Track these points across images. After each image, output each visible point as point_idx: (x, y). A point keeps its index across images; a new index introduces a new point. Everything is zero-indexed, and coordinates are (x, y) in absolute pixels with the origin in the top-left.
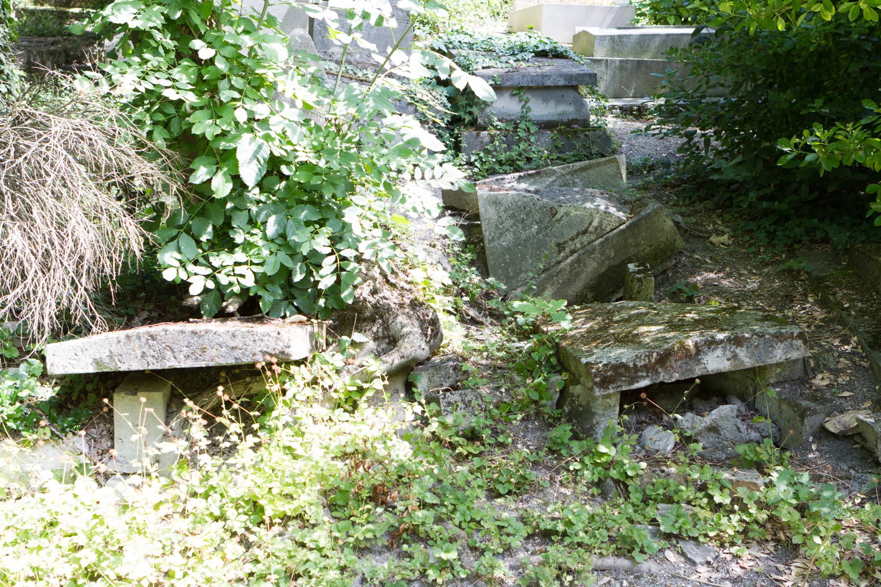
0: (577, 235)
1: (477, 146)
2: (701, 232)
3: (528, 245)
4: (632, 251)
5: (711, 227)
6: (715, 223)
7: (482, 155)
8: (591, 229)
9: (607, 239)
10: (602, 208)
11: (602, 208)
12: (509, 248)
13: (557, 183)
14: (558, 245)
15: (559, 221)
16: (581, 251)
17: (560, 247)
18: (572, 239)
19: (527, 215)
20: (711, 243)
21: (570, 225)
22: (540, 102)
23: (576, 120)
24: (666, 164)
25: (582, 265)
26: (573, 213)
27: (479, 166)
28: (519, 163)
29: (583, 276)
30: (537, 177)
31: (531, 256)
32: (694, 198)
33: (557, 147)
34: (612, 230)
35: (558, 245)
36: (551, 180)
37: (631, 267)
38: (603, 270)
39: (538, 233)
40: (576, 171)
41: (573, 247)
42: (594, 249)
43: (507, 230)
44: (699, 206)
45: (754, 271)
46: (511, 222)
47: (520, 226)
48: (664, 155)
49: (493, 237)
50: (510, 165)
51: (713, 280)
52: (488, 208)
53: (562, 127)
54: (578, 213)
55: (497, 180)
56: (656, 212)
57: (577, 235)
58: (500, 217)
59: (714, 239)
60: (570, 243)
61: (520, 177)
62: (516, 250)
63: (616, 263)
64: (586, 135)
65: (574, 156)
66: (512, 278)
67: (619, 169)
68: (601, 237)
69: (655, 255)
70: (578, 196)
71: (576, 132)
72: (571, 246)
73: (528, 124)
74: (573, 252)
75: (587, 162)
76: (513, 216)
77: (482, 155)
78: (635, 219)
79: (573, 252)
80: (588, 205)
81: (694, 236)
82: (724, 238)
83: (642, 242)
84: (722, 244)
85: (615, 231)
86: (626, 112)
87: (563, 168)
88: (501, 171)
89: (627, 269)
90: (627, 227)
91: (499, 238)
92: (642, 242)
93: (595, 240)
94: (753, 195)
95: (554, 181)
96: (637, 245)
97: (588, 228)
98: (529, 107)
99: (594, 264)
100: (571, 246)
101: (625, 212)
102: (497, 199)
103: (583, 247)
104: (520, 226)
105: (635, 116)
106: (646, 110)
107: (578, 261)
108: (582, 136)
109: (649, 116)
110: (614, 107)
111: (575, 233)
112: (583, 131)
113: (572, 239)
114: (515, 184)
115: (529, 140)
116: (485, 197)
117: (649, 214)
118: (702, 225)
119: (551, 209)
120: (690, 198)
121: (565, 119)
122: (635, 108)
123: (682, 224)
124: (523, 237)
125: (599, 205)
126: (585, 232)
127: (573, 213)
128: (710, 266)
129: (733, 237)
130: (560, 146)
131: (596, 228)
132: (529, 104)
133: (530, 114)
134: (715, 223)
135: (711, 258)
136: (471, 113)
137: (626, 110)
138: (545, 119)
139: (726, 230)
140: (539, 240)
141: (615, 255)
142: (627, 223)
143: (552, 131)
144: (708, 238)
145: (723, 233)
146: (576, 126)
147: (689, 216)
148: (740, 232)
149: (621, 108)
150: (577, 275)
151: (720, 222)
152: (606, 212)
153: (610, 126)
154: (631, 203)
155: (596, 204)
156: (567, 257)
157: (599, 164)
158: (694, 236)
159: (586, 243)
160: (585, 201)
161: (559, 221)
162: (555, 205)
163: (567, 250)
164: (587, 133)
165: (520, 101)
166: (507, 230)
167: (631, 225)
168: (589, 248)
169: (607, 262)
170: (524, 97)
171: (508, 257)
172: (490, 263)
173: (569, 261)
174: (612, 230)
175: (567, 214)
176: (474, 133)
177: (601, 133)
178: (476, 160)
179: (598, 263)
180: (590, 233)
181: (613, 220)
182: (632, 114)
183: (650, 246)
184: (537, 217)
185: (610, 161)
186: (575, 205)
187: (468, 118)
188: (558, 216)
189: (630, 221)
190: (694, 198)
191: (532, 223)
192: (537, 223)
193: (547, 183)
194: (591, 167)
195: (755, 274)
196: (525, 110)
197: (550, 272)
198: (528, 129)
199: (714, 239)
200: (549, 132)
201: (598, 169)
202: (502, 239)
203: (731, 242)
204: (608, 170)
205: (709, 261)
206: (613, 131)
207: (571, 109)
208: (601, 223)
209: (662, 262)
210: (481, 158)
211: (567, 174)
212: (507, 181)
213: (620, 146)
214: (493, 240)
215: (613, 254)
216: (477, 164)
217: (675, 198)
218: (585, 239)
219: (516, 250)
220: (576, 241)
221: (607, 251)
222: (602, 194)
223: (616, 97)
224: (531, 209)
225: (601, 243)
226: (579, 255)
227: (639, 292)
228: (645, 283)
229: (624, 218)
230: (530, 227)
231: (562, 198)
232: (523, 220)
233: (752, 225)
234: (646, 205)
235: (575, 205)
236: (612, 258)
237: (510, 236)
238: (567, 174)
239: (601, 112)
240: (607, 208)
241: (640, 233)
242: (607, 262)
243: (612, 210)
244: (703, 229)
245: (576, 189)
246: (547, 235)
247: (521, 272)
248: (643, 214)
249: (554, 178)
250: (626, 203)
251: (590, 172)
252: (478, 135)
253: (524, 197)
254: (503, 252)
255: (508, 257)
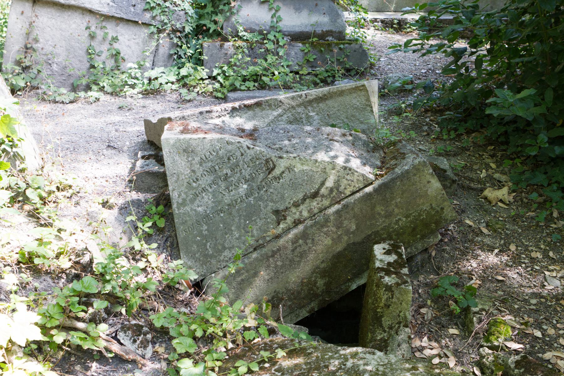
0: (304, 200)
1: (220, 58)
2: (471, 180)
3: (234, 212)
4: (381, 223)
5: (483, 174)
6: (488, 167)
7: (225, 68)
8: (323, 191)
9: (346, 206)
10: (340, 161)
11: (340, 161)
12: (207, 216)
13: (285, 118)
14: (277, 212)
15: (277, 178)
16: (309, 223)
17: (280, 215)
18: (296, 205)
19: (232, 170)
20: (486, 198)
21: (294, 186)
22: (292, 11)
23: (331, 31)
24: (428, 88)
25: (309, 241)
26: (299, 167)
27: (221, 80)
28: (264, 78)
29: (311, 256)
30: (257, 110)
31: (238, 228)
32: (461, 130)
33: (308, 61)
34: (353, 193)
35: (277, 212)
36: (275, 113)
37: (378, 250)
38: (339, 248)
39: (247, 196)
40: (310, 102)
41: (297, 216)
42: (327, 220)
43: (204, 190)
44: (467, 141)
45: (551, 254)
46: (209, 179)
47: (223, 185)
48: (423, 71)
49: (184, 200)
50: (255, 81)
51: (494, 267)
52: (177, 158)
53: (315, 39)
54: (305, 168)
55: (201, 113)
56: (416, 169)
57: (304, 200)
58: (194, 171)
59: (489, 193)
60: (294, 210)
61: (234, 109)
62: (218, 218)
63: (358, 239)
64: (340, 49)
65: (327, 71)
66: (212, 256)
67: (368, 100)
68: (338, 202)
69: (414, 229)
70: (309, 140)
71: (329, 45)
72: (294, 214)
73: (277, 35)
74: (297, 223)
75: (326, 89)
76: (213, 171)
77: (225, 68)
78: (386, 179)
79: (297, 223)
80: (322, 156)
81: (463, 187)
82: (503, 193)
83: (396, 210)
84: (501, 201)
85: (358, 195)
86: (387, 25)
87: (293, 98)
88: (243, 88)
89: (370, 257)
90: (376, 190)
91: (192, 201)
92: (396, 210)
93: (329, 207)
94: (543, 137)
95: (280, 116)
96: (389, 215)
97: (319, 189)
98: (279, 17)
99: (328, 241)
100: (294, 214)
101: (373, 166)
102: (189, 145)
103: (312, 216)
104: (223, 185)
105: (395, 29)
106: (406, 23)
107: (304, 235)
108: (336, 50)
109: (409, 30)
110: (375, 20)
111: (301, 196)
112: (337, 44)
113: (296, 205)
114: (227, 119)
115: (278, 54)
116: (172, 142)
117: (407, 172)
118: (472, 170)
119: (267, 161)
120: (456, 130)
121: (319, 30)
122: (396, 21)
123: (449, 173)
124: (227, 199)
125: (336, 157)
126: (315, 195)
127: (299, 167)
128: (487, 241)
129: (514, 191)
130: (311, 60)
131: (331, 190)
132: (279, 13)
133: (280, 24)
134: (488, 167)
135: (487, 226)
136: (216, 22)
137: (386, 23)
138: (298, 29)
139: (503, 178)
140: (249, 205)
141: (357, 229)
142: (376, 184)
143: (304, 44)
144: (482, 190)
145: (499, 185)
146: (330, 38)
147: (455, 155)
148: (523, 185)
149: (382, 21)
150: (302, 255)
151: (493, 166)
152: (345, 168)
153: (369, 38)
154: (382, 148)
155: (332, 154)
156: (288, 230)
157: (341, 93)
158: (463, 187)
159: (316, 211)
160: (317, 149)
161: (277, 178)
162: (273, 155)
163: (289, 220)
164: (342, 46)
165: (270, 9)
166: (204, 190)
167: (380, 186)
168: (320, 218)
169: (346, 238)
170: (275, 6)
171: (205, 227)
172: (181, 235)
173: (291, 236)
174: (353, 193)
175: (289, 169)
176: (218, 43)
177: (357, 47)
178: (218, 74)
179: (333, 239)
180: (323, 196)
181: (355, 178)
182: (392, 27)
183: (407, 217)
184: (246, 173)
185: (357, 89)
186: (303, 155)
187: (213, 27)
188: (277, 172)
189: (380, 181)
190: (461, 130)
191: (239, 181)
192: (246, 181)
193: (271, 118)
194: (331, 97)
195: (553, 261)
196: (275, 20)
197: (264, 250)
198: (278, 40)
199: (489, 193)
200: (300, 45)
201: (340, 99)
202: (197, 202)
203: (511, 198)
204: (354, 101)
205: (485, 231)
206: (371, 44)
207: (325, 19)
208: (337, 183)
209: (423, 237)
210: (224, 72)
211: (299, 106)
212: (215, 114)
213: (379, 60)
214: (183, 204)
215: (354, 227)
216: (219, 78)
217: (438, 129)
218: (315, 204)
219: (218, 218)
220: (302, 207)
221: (346, 223)
222: (344, 135)
223: (379, 11)
224: (238, 162)
225: (338, 212)
226: (306, 228)
227: (388, 306)
228: (397, 293)
229: (372, 177)
230: (237, 187)
231: (286, 142)
232: (226, 177)
233: (541, 178)
234: (403, 156)
235: (303, 155)
236: (353, 233)
237: (207, 199)
238: (299, 106)
239: (358, 24)
240: (347, 161)
241: (392, 199)
242: (346, 238)
243: (355, 163)
244: (473, 175)
245: (308, 128)
246: (261, 199)
247: (224, 248)
248: (398, 171)
249: (280, 111)
250: (376, 148)
251: (330, 102)
252: (221, 46)
253: (228, 143)
254: (198, 222)
255: (205, 227)
